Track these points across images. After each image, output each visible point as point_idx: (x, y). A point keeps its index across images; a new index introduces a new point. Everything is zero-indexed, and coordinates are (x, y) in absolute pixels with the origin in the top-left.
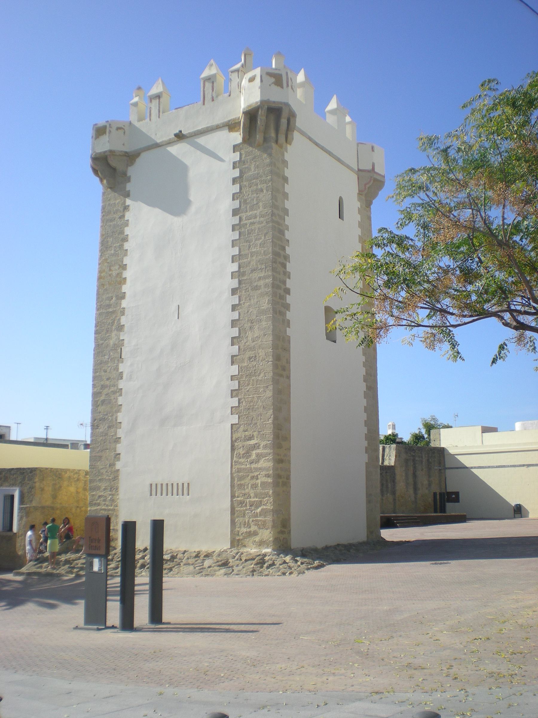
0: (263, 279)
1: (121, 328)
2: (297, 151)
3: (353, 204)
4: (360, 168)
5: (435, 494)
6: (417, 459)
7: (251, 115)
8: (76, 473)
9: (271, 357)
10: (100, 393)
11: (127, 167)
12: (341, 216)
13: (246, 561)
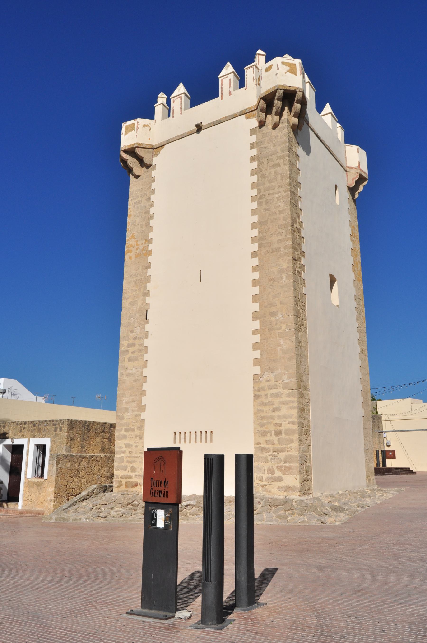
0: (283, 240)
5: (377, 452)
9: (292, 311)
10: (127, 351)
11: (153, 158)
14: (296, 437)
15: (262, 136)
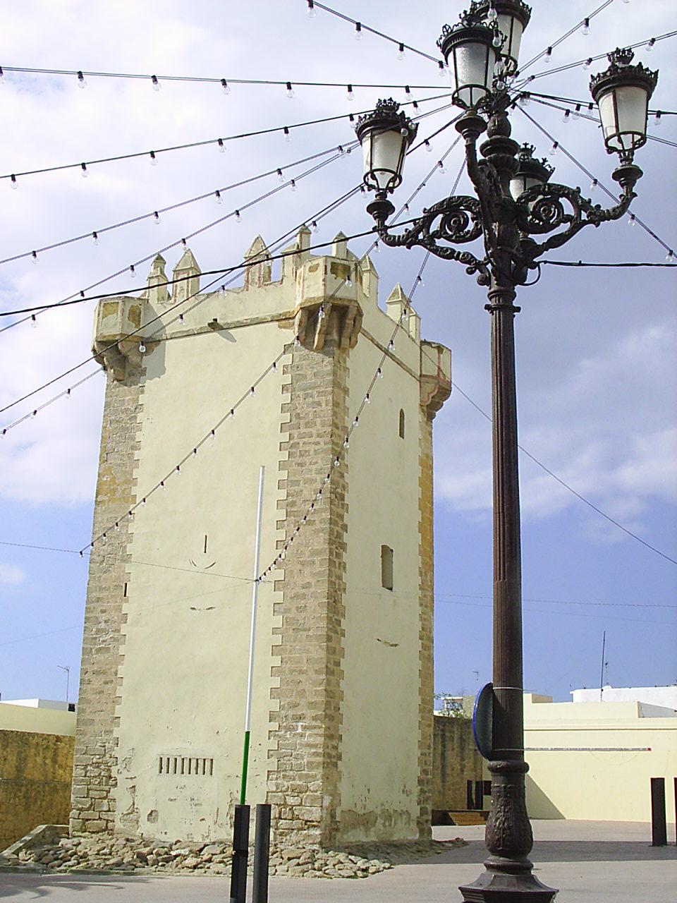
1: (126, 559)
2: (362, 355)
3: (415, 417)
4: (424, 373)
5: (469, 782)
6: (447, 734)
7: (310, 312)
8: (45, 739)
12: (402, 435)
13: (289, 859)
14: (319, 772)
15: (300, 359)
